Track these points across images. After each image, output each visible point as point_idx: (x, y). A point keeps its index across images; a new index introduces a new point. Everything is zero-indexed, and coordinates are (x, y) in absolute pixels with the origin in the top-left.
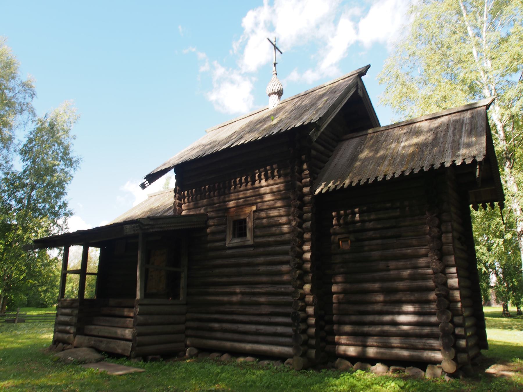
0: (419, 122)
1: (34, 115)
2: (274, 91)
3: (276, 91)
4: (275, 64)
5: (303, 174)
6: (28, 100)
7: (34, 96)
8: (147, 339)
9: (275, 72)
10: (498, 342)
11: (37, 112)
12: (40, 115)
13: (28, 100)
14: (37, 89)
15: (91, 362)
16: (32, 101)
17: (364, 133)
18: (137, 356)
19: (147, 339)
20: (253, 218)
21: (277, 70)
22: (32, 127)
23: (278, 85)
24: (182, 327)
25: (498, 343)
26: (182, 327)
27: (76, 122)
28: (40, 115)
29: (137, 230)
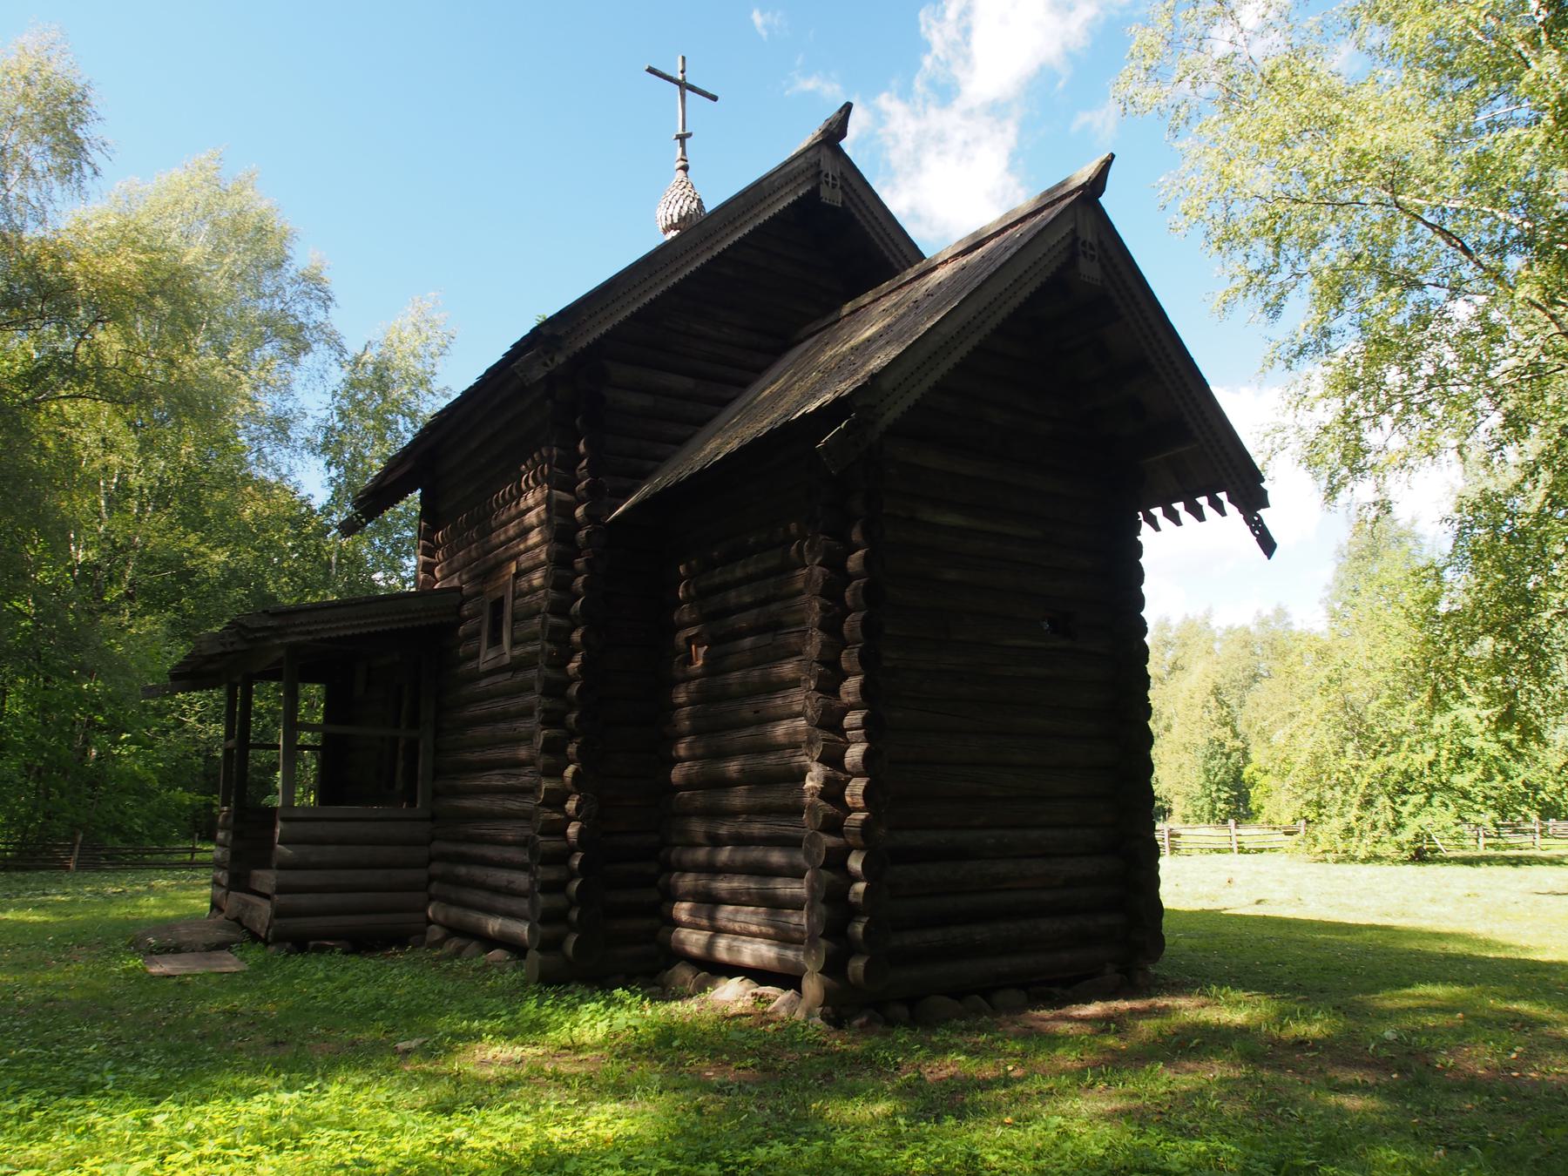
0: (942, 263)
1: (342, 351)
2: (669, 222)
3: (676, 221)
4: (682, 138)
5: (578, 472)
6: (319, 315)
7: (328, 303)
8: (304, 900)
9: (681, 163)
10: (1439, 936)
11: (347, 344)
12: (353, 347)
13: (319, 315)
14: (334, 288)
15: (193, 951)
16: (327, 318)
17: (832, 318)
18: (279, 939)
19: (304, 900)
20: (514, 592)
21: (688, 157)
22: (337, 376)
23: (681, 202)
24: (420, 875)
25: (1436, 947)
26: (420, 875)
27: (447, 352)
28: (353, 347)
29: (232, 643)
